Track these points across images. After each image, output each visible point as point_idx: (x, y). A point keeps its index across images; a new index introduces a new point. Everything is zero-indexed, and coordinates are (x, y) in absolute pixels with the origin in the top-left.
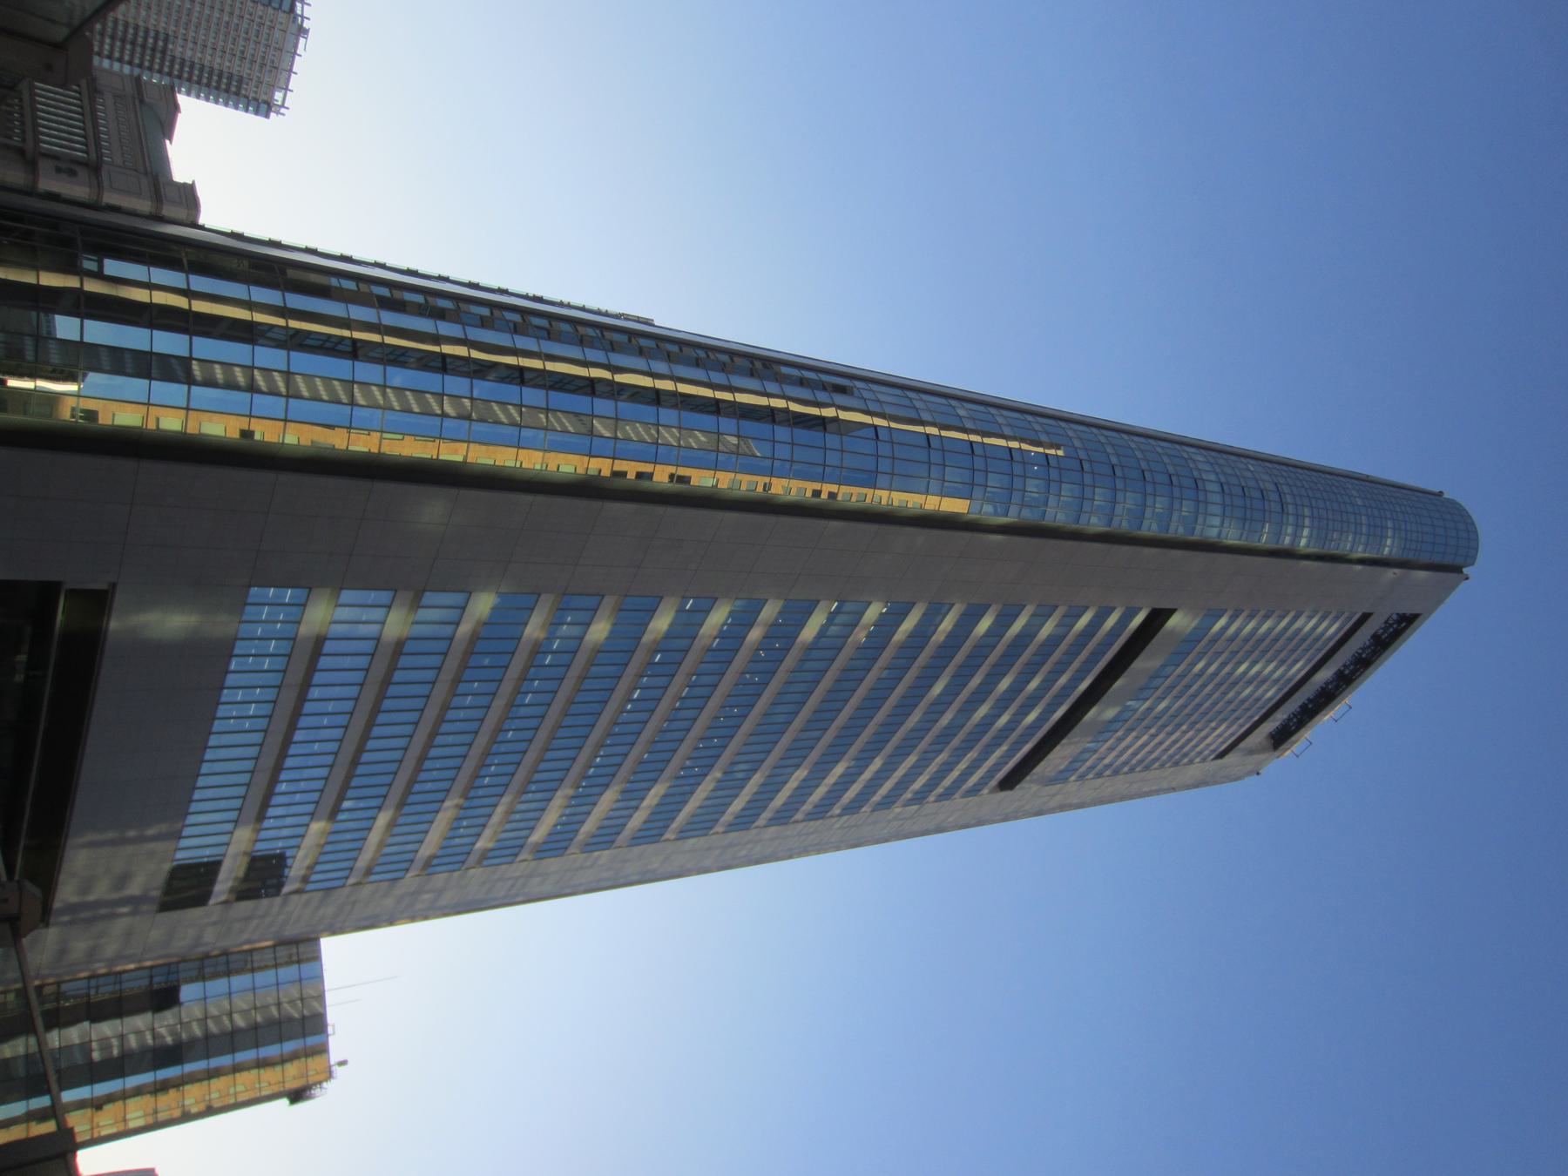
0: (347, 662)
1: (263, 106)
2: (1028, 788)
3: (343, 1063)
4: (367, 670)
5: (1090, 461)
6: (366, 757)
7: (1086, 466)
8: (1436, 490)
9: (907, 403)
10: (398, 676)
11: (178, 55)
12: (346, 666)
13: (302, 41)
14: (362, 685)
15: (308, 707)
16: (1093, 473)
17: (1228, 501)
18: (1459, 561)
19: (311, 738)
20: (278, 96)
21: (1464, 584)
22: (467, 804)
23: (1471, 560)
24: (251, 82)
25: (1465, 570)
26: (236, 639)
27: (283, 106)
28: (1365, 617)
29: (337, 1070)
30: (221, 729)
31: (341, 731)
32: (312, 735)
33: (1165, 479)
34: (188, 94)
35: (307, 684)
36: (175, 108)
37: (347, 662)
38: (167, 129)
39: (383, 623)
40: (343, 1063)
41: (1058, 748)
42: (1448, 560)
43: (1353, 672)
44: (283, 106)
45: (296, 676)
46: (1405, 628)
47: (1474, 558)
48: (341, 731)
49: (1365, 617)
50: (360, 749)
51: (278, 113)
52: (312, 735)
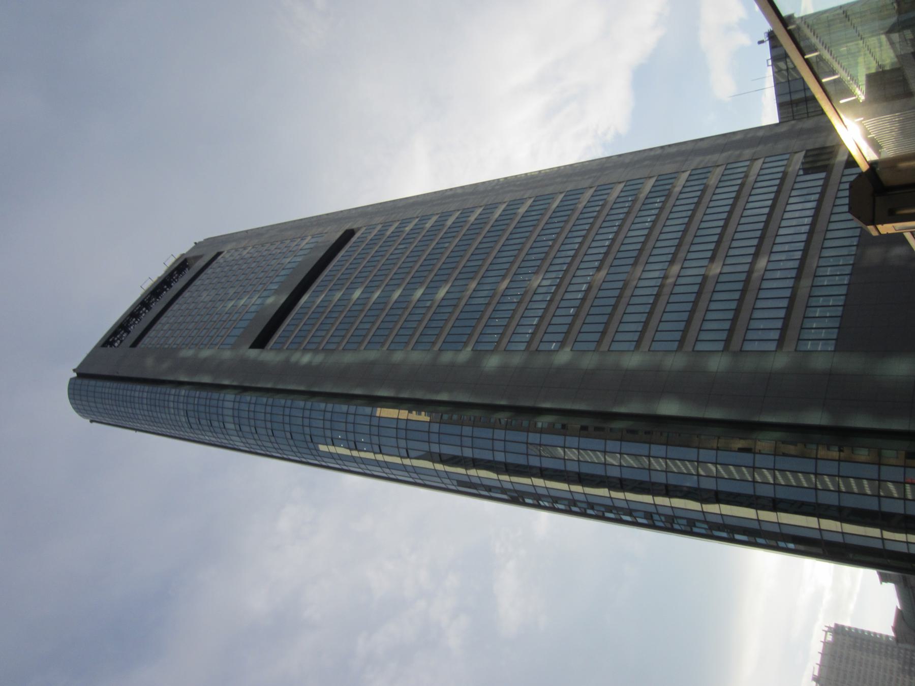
0: (766, 314)
1: (838, 631)
2: (308, 250)
3: (761, 42)
4: (757, 299)
5: (306, 442)
6: (755, 242)
7: (308, 438)
8: (94, 424)
9: (422, 477)
10: (737, 296)
11: (896, 661)
12: (774, 286)
13: (816, 673)
14: (760, 289)
15: (801, 246)
16: (304, 434)
17: (221, 417)
18: (79, 381)
19: (792, 253)
20: (830, 638)
21: (75, 367)
22: (705, 181)
23: (72, 382)
24: (846, 646)
25: (75, 375)
26: (834, 351)
27: (826, 632)
28: (134, 345)
29: (764, 37)
30: (853, 239)
31: (777, 242)
32: (801, 221)
33: (259, 430)
34: (887, 637)
35: (811, 233)
36: (895, 629)
37: (766, 314)
38: (901, 617)
39: (769, 261)
40: (761, 42)
41: (318, 259)
42: (86, 382)
43: (140, 309)
44: (826, 632)
45: (817, 238)
46: (111, 337)
47: (70, 384)
48: (757, 306)
49: (134, 345)
50: (741, 301)
51: (829, 628)
52: (801, 221)
